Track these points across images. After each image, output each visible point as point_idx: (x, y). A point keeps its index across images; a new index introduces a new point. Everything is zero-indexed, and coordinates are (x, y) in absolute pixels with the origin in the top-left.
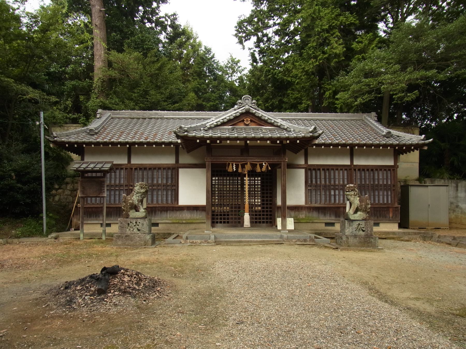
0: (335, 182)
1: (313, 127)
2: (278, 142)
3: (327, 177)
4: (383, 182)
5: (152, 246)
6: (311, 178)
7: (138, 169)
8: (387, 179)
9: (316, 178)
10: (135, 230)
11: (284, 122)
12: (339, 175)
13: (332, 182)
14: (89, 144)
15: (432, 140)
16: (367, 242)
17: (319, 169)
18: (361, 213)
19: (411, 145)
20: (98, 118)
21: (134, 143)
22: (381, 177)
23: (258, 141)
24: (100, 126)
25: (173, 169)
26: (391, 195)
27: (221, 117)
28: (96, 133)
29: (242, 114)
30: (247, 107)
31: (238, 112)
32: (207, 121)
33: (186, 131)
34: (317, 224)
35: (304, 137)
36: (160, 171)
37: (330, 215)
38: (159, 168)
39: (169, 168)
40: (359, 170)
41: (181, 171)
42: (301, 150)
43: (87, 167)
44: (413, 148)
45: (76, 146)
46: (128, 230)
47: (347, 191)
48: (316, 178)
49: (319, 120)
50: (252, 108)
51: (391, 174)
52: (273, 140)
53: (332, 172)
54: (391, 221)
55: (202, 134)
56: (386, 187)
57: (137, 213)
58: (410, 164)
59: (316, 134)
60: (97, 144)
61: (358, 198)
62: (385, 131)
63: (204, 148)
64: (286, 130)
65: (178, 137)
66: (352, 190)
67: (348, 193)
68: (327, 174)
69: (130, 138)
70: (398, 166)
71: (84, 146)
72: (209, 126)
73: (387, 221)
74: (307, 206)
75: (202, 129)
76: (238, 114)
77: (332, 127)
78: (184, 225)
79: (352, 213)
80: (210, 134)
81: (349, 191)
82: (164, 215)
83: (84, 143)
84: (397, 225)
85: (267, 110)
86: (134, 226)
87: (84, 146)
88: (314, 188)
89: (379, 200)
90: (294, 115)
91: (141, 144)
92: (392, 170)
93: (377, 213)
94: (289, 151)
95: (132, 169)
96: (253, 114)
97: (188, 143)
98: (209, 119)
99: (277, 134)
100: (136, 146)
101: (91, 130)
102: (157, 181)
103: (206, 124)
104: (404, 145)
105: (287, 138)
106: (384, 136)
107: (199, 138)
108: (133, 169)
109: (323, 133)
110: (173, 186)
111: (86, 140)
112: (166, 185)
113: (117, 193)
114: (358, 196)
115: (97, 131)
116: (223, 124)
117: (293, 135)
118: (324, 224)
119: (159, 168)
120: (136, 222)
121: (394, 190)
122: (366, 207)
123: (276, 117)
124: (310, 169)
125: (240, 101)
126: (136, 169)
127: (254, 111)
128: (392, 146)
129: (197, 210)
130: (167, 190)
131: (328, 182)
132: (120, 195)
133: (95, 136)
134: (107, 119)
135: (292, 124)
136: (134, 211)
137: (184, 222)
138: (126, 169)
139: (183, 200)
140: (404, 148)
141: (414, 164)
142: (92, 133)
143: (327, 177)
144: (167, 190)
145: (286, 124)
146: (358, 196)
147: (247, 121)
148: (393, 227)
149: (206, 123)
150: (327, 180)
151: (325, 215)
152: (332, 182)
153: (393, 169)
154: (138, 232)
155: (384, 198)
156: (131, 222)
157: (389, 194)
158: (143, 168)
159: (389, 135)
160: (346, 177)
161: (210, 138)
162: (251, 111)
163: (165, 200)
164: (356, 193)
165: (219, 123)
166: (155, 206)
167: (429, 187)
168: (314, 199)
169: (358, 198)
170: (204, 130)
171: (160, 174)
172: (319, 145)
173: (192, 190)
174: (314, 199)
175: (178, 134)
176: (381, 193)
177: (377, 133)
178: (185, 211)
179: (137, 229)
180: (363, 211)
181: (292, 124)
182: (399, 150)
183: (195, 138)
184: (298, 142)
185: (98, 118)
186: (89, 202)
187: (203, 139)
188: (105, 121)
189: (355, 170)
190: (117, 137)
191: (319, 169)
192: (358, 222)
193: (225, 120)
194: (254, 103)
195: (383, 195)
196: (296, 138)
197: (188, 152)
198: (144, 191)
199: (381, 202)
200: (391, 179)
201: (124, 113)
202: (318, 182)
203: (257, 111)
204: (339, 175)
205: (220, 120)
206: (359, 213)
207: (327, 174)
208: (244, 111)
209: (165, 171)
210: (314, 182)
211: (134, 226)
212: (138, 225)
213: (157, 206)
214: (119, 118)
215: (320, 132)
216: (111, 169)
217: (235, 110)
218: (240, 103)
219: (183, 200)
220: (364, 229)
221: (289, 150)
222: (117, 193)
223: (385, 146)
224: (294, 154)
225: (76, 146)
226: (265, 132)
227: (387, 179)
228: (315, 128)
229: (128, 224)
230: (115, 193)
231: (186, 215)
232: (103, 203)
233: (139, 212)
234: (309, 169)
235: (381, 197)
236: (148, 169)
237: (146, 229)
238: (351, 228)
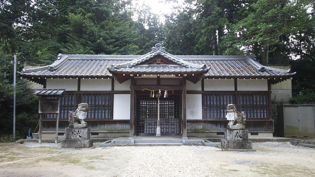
0: (223, 103)
1: (204, 65)
2: (179, 75)
3: (218, 100)
4: (260, 103)
5: (90, 148)
6: (207, 100)
7: (85, 94)
8: (263, 101)
9: (210, 101)
10: (78, 137)
11: (185, 62)
12: (227, 99)
13: (222, 103)
14: (49, 77)
15: (295, 72)
16: (243, 145)
17: (212, 95)
18: (239, 124)
19: (280, 76)
20: (59, 60)
21: (82, 77)
22: (258, 100)
23: (172, 75)
24: (59, 65)
25: (110, 94)
26: (266, 112)
27: (141, 58)
28: (55, 70)
29: (155, 56)
30: (158, 51)
31: (152, 55)
32: (131, 61)
33: (116, 68)
34: (213, 134)
35: (197, 72)
36: (100, 96)
37: (221, 127)
38: (100, 94)
39: (107, 94)
40: (241, 95)
41: (115, 96)
42: (186, 80)
43: (51, 93)
44: (281, 78)
45: (39, 78)
46: (72, 136)
47: (228, 109)
48: (210, 101)
49: (226, 60)
50: (162, 52)
51: (266, 97)
52: (176, 74)
53: (255, 96)
54: (267, 131)
55: (128, 70)
56: (262, 107)
57: (80, 124)
58: (284, 90)
59: (206, 70)
60: (55, 77)
61: (237, 114)
62: (260, 66)
63: (129, 81)
64: (185, 67)
65: (110, 72)
66: (232, 108)
67: (228, 110)
68: (218, 98)
69: (79, 73)
70: (271, 92)
71: (46, 78)
72: (132, 65)
73: (264, 131)
74: (204, 120)
75: (127, 66)
76: (152, 56)
77: (216, 66)
78: (114, 134)
79: (232, 125)
80: (133, 70)
81: (229, 109)
82: (102, 127)
83: (46, 76)
84: (272, 135)
85: (173, 53)
86: (77, 134)
87: (46, 78)
88: (209, 108)
89: (257, 116)
90: (196, 57)
91: (87, 77)
92: (266, 94)
93: (253, 125)
94: (111, 80)
95: (80, 94)
96: (163, 57)
97: (118, 76)
98: (133, 60)
99: (178, 70)
100: (84, 78)
101: (51, 68)
102: (99, 103)
103: (130, 63)
104: (274, 77)
105: (186, 73)
106: (260, 70)
107: (124, 73)
108: (82, 94)
109: (210, 68)
110: (109, 106)
111: (47, 75)
112: (104, 106)
113: (66, 111)
114: (236, 112)
115: (55, 68)
116: (142, 63)
117: (189, 70)
118: (216, 134)
119: (100, 94)
120: (78, 131)
121: (269, 109)
122: (242, 120)
123: (180, 59)
124: (206, 94)
125: (154, 47)
126: (83, 94)
127: (163, 54)
128: (265, 77)
129: (126, 124)
130: (105, 110)
131: (218, 103)
132: (68, 113)
133: (54, 72)
134: (64, 60)
135: (192, 64)
136: (77, 123)
137: (116, 132)
138: (76, 94)
139: (116, 117)
140: (275, 79)
141: (289, 91)
142: (51, 69)
143: (218, 100)
144: (105, 110)
145: (186, 63)
146: (236, 112)
147: (159, 61)
148: (270, 136)
149: (129, 62)
150: (218, 102)
151: (217, 126)
152: (222, 103)
153: (267, 94)
154: (80, 138)
155: (261, 115)
156: (75, 131)
157: (265, 111)
158: (88, 94)
159: (263, 70)
160: (231, 100)
161: (132, 73)
162: (161, 54)
163: (104, 117)
164: (234, 110)
165: (139, 63)
166: (96, 120)
167: (299, 107)
168: (208, 115)
169: (237, 114)
170: (129, 67)
171: (100, 98)
172: (210, 77)
173: (122, 109)
174: (208, 115)
175: (110, 70)
176: (259, 111)
177: (255, 69)
178: (118, 124)
179: (79, 136)
180: (240, 123)
181: (192, 64)
182: (273, 80)
183: (122, 73)
184: (193, 75)
185: (59, 60)
186: (48, 117)
187: (128, 74)
188: (63, 61)
189: (238, 95)
190: (85, 72)
191: (212, 95)
192: (237, 131)
193: (144, 61)
194: (164, 49)
195: (260, 113)
196: (192, 72)
197: (121, 82)
198: (85, 109)
199: (259, 117)
200: (266, 101)
201: (78, 56)
202: (212, 103)
203: (165, 54)
204: (227, 99)
205: (140, 60)
206: (237, 124)
207: (218, 98)
208: (156, 54)
209: (104, 96)
210: (208, 103)
211: (77, 134)
212: (80, 133)
213: (98, 120)
214: (74, 60)
215: (208, 68)
216: (63, 94)
217: (151, 53)
218: (154, 49)
219: (116, 117)
220: (241, 136)
221: (131, 80)
222: (66, 111)
223: (260, 77)
224: (195, 84)
225: (39, 78)
226: (171, 69)
227: (263, 101)
228: (205, 66)
229: (73, 132)
230: (64, 111)
231: (119, 127)
232: (56, 119)
233: (81, 124)
234: (206, 95)
235: (259, 114)
236: (92, 94)
237: (86, 136)
238: (231, 135)
